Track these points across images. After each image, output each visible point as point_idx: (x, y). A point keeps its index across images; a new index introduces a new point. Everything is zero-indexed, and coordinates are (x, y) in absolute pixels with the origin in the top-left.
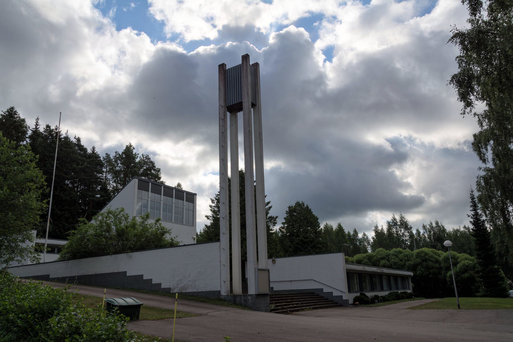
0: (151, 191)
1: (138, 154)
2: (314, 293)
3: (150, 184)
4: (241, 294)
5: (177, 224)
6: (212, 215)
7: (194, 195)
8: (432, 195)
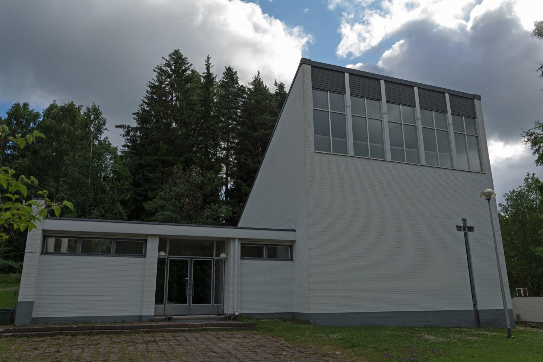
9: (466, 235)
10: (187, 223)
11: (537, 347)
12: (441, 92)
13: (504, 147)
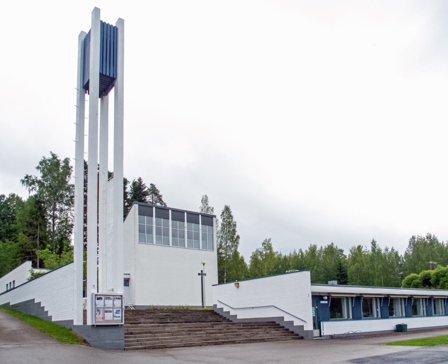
0: (201, 223)
1: (135, 180)
2: (274, 322)
3: (154, 208)
4: (214, 326)
5: (161, 246)
6: (25, 201)
7: (212, 217)
8: (38, 181)
9: (202, 277)
10: (322, 283)
11: (45, 330)
12: (183, 212)
13: (267, 245)
